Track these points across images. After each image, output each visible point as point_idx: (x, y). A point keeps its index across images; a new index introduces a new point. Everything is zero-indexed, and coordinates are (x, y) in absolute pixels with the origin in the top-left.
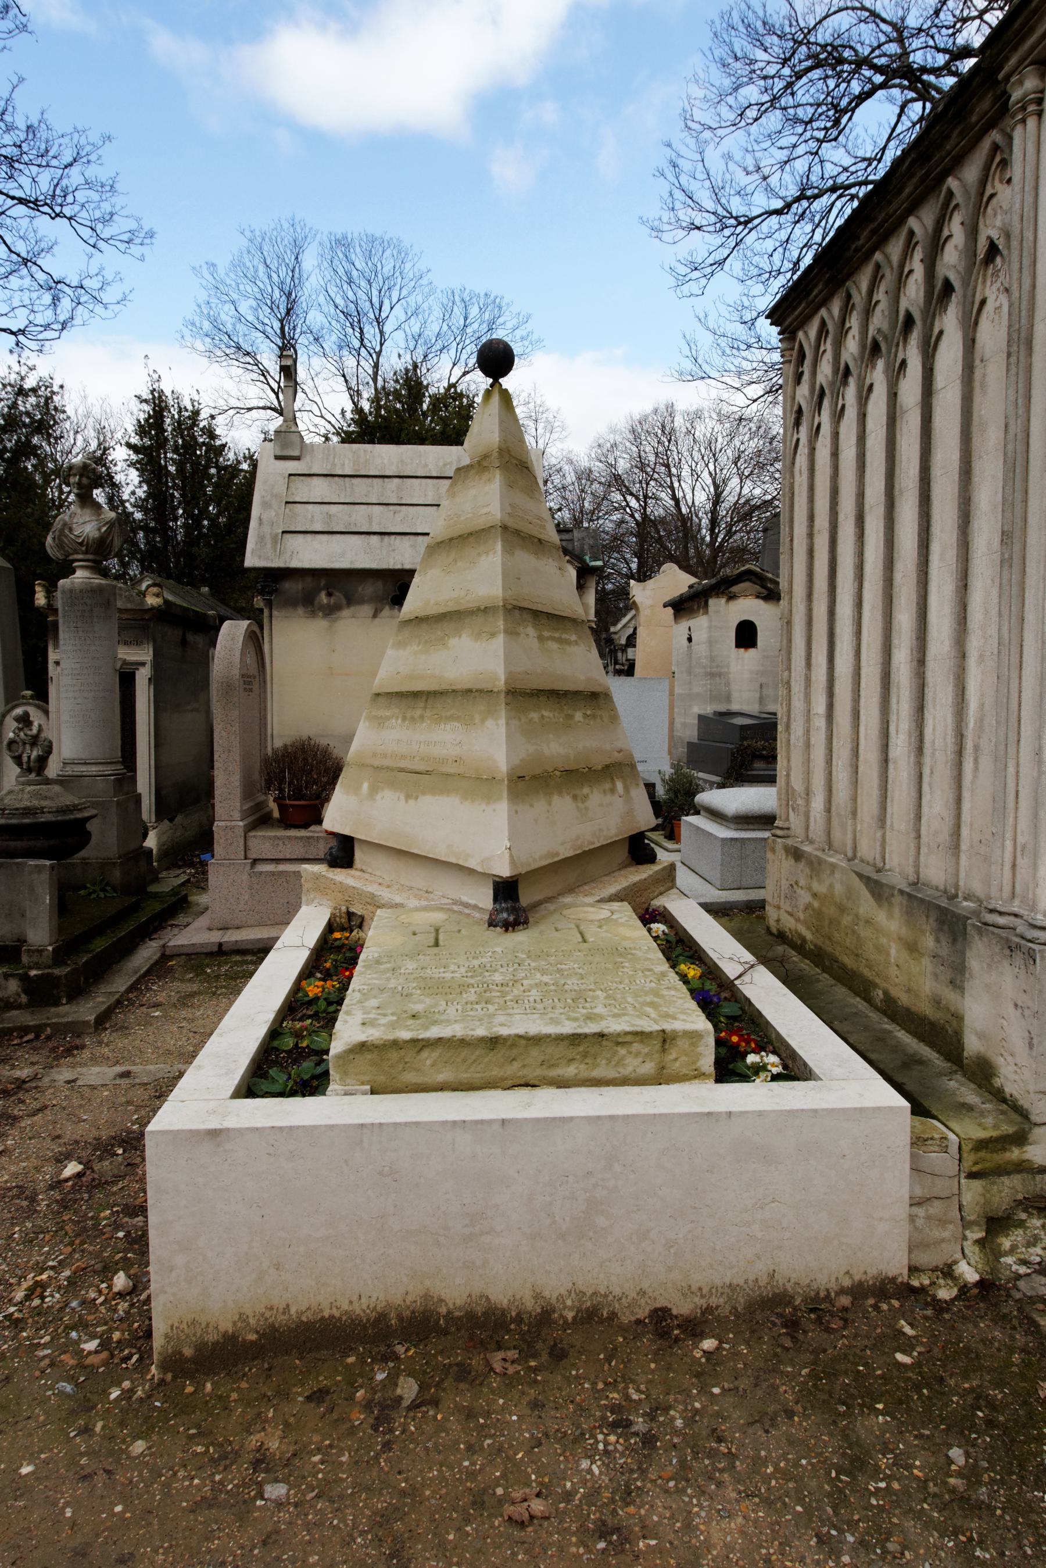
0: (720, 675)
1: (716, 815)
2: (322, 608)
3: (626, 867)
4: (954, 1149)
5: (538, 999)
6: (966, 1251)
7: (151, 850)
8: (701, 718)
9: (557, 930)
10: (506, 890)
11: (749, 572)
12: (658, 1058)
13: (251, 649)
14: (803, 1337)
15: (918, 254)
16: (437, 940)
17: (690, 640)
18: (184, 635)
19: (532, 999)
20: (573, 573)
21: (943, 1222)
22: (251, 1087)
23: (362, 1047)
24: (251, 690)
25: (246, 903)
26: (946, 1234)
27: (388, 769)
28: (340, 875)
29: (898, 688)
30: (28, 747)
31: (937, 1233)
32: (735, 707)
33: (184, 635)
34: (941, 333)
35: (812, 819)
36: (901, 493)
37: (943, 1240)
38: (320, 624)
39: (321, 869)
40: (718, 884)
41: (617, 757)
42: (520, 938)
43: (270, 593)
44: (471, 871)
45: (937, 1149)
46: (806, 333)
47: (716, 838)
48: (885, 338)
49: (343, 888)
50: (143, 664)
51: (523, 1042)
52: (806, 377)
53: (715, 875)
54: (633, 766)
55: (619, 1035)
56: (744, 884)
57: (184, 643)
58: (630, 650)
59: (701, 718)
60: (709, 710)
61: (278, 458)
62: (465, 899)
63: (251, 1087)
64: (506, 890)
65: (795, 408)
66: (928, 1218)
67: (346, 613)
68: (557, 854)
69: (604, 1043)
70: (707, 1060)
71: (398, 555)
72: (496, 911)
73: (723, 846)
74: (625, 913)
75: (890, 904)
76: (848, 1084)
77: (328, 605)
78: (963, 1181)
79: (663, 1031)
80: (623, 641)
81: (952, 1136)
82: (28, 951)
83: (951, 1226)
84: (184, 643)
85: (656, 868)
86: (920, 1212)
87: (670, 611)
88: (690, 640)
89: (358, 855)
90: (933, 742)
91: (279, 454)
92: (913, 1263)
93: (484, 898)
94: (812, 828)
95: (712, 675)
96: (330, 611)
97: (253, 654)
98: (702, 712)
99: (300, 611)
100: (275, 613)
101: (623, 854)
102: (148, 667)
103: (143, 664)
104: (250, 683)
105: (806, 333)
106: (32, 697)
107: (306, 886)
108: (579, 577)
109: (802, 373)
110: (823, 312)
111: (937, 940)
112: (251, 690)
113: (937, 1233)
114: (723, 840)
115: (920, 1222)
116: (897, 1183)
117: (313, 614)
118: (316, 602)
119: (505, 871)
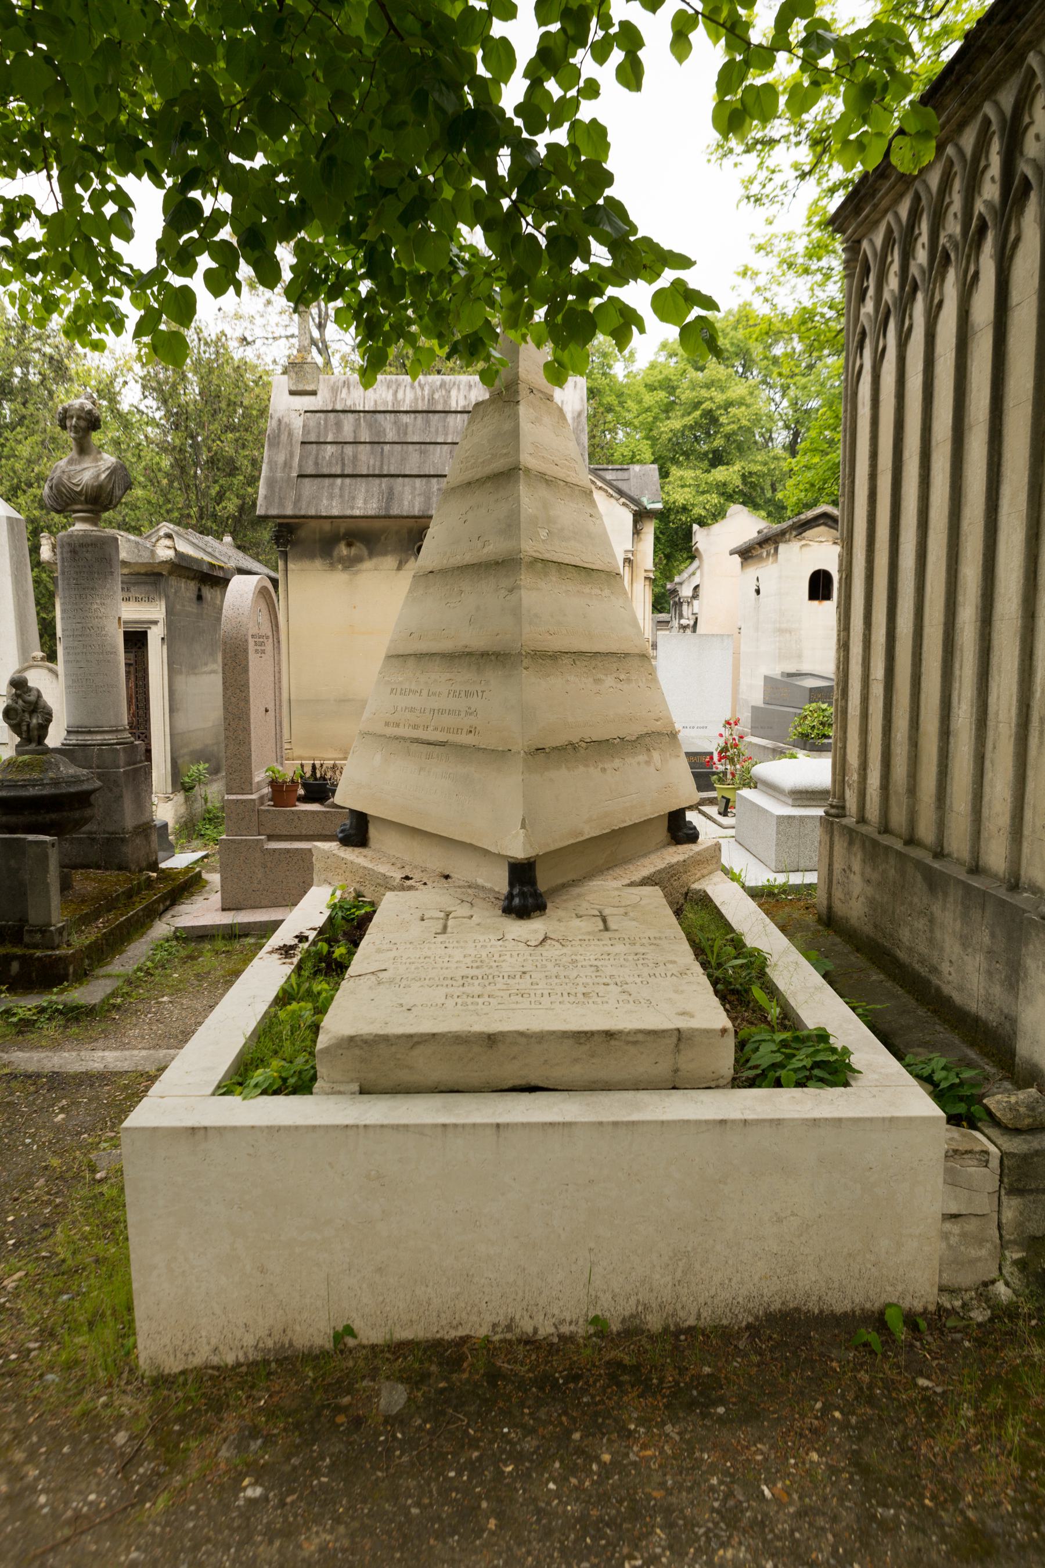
0: (790, 631)
1: (771, 788)
2: (341, 560)
3: (664, 847)
4: (994, 1163)
5: (546, 992)
6: (1004, 1271)
7: (165, 826)
8: (767, 679)
9: (578, 916)
10: (522, 873)
11: (825, 515)
12: (662, 1061)
13: (263, 606)
14: (790, 1361)
15: (995, 146)
16: (445, 927)
17: (758, 592)
18: (200, 590)
19: (539, 992)
20: (629, 517)
21: (981, 1242)
22: (237, 1080)
23: (352, 1041)
24: (263, 652)
25: (260, 882)
26: (983, 1252)
27: (404, 739)
28: (351, 855)
29: (962, 651)
30: (27, 715)
31: (974, 1252)
32: (805, 668)
33: (200, 590)
34: (1018, 239)
35: (868, 798)
36: (970, 428)
37: (979, 1259)
38: (339, 578)
39: (332, 846)
40: (773, 866)
41: (657, 726)
42: (534, 928)
43: (285, 545)
44: (486, 852)
45: (976, 1163)
46: (871, 241)
47: (772, 815)
48: (956, 247)
49: (354, 869)
50: (155, 623)
51: (523, 1040)
52: (871, 292)
53: (771, 855)
54: (673, 735)
55: (629, 1033)
56: (802, 866)
57: (200, 598)
58: (695, 602)
59: (767, 679)
60: (776, 670)
61: (292, 393)
62: (480, 881)
63: (237, 1080)
64: (522, 873)
65: (858, 330)
66: (964, 1235)
67: (368, 565)
68: (581, 834)
69: (613, 1042)
70: (725, 1060)
71: (409, 500)
72: (510, 897)
73: (778, 824)
74: (654, 895)
75: (946, 894)
76: (887, 1090)
77: (348, 556)
78: (1004, 1198)
79: (678, 1030)
80: (690, 593)
81: (992, 1148)
82: (31, 931)
83: (988, 1245)
84: (200, 598)
85: (695, 848)
86: (954, 1228)
87: (737, 558)
88: (758, 592)
89: (373, 832)
90: (997, 714)
91: (294, 388)
92: (944, 1282)
93: (499, 881)
94: (868, 807)
95: (781, 631)
96: (350, 563)
97: (265, 611)
98: (770, 673)
99: (318, 563)
100: (291, 566)
101: (662, 832)
102: (161, 625)
103: (155, 623)
104: (262, 644)
105: (871, 241)
106: (42, 659)
107: (318, 865)
108: (635, 522)
109: (867, 288)
110: (890, 217)
111: (993, 935)
112: (263, 652)
113: (974, 1252)
114: (779, 817)
115: (953, 1241)
116: (929, 1197)
117: (332, 566)
118: (335, 553)
119: (519, 851)
